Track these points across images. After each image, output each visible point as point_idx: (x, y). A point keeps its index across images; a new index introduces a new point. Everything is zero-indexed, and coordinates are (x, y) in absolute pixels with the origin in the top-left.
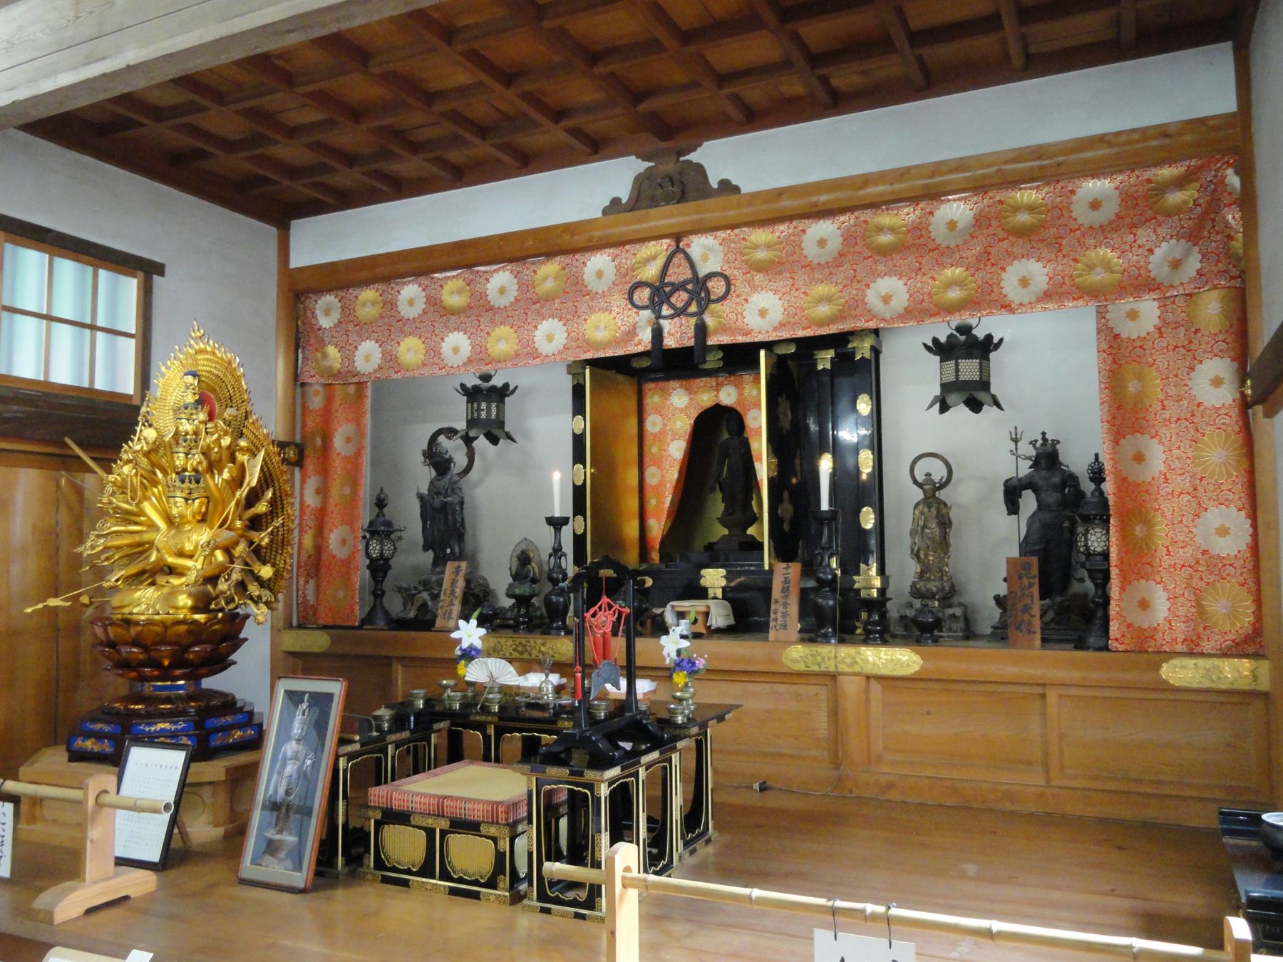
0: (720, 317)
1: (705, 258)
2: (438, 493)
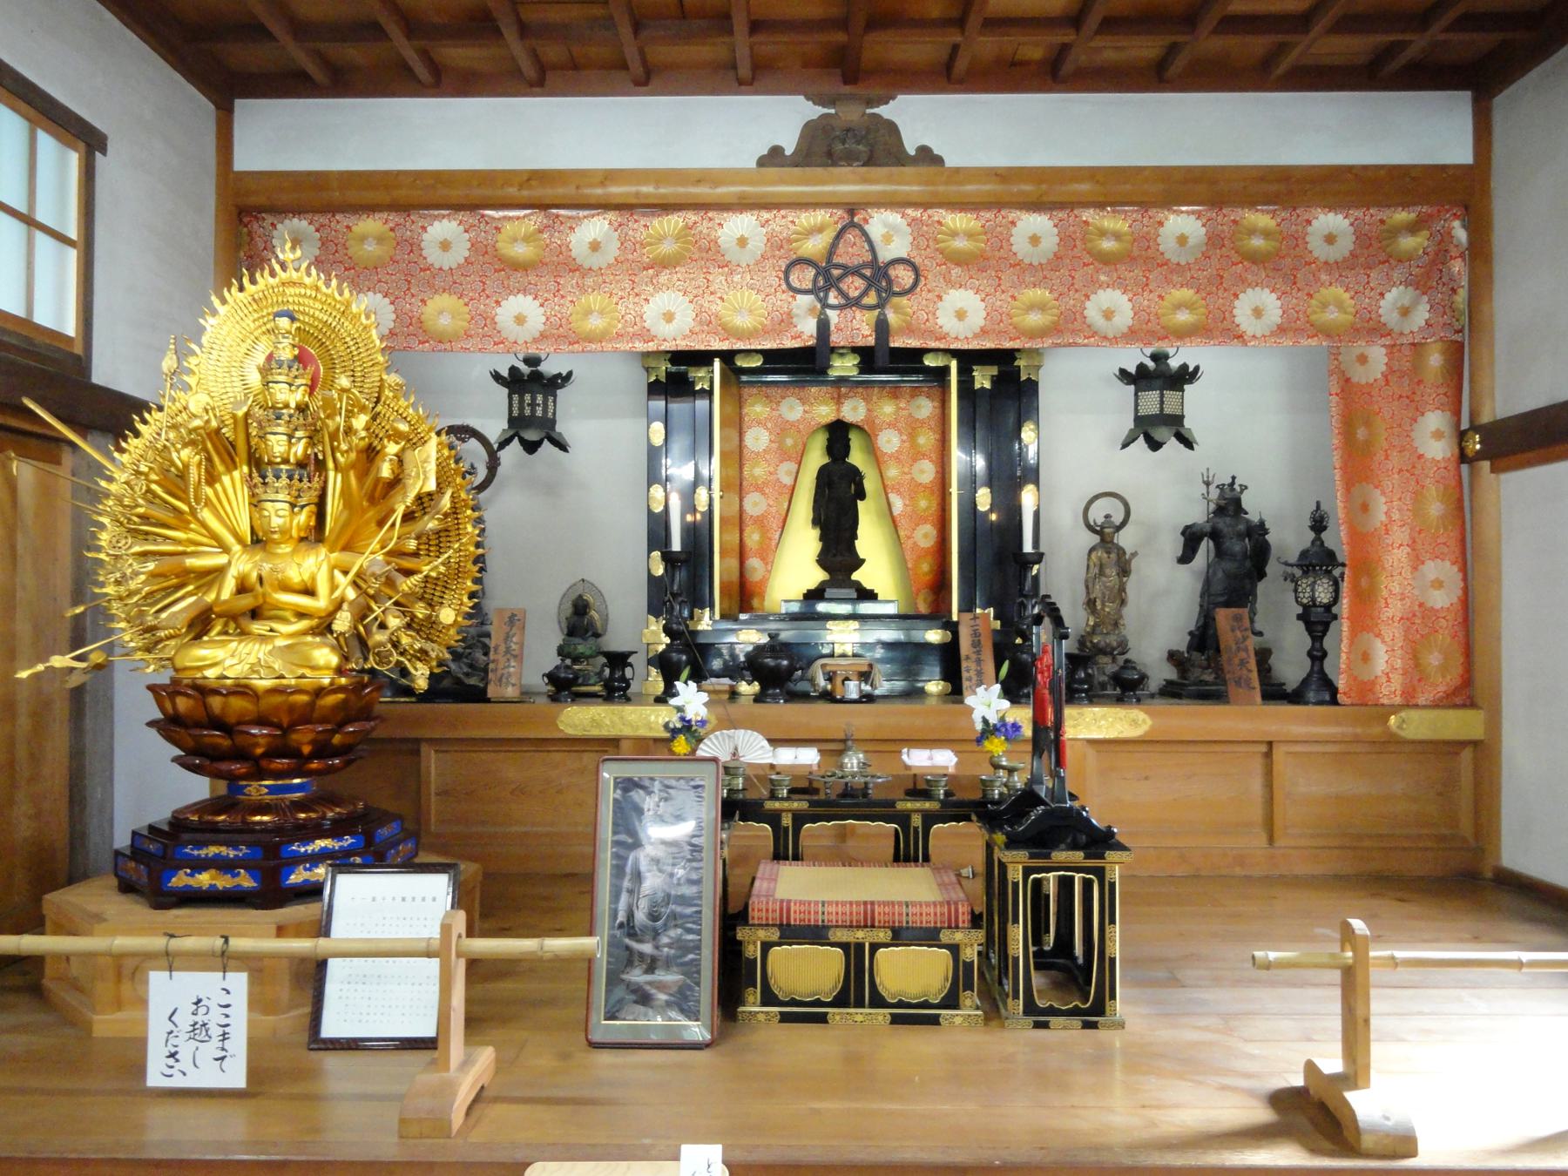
0: (905, 314)
1: (887, 239)
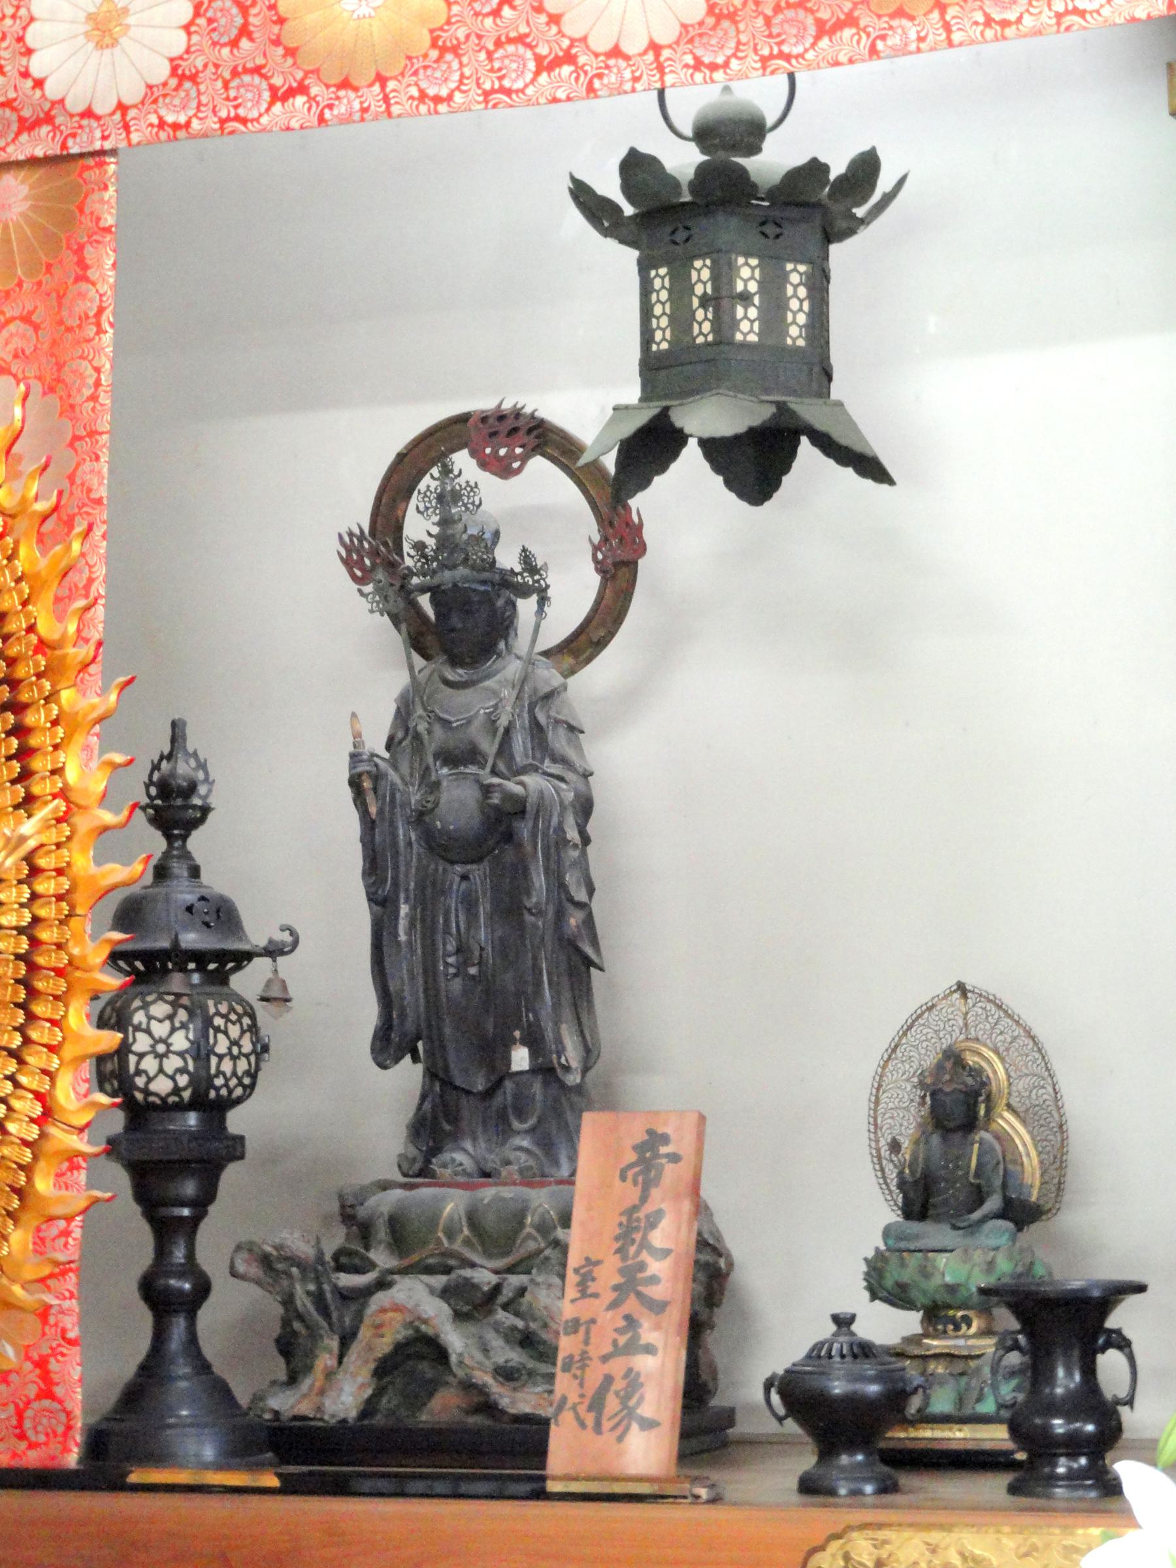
2: (460, 757)
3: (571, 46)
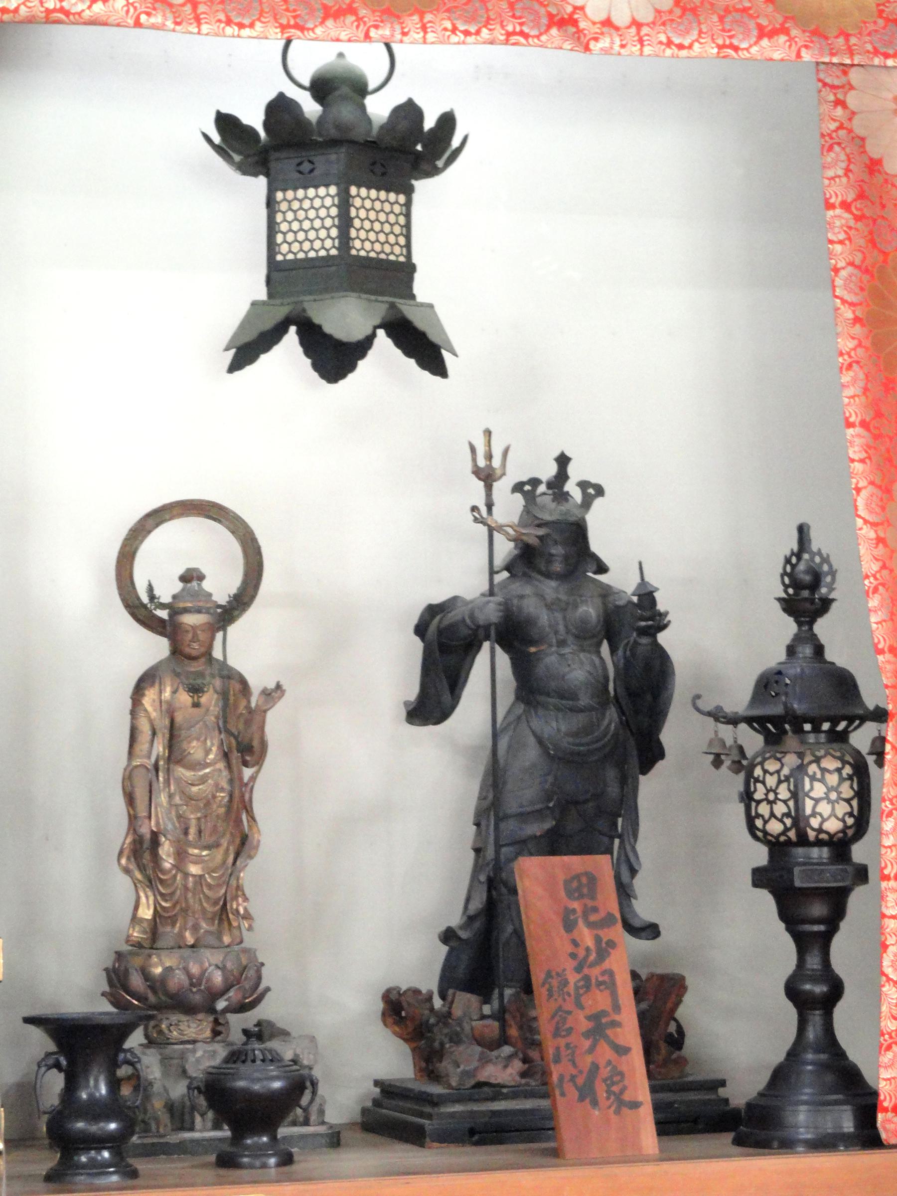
3: (573, 13)
